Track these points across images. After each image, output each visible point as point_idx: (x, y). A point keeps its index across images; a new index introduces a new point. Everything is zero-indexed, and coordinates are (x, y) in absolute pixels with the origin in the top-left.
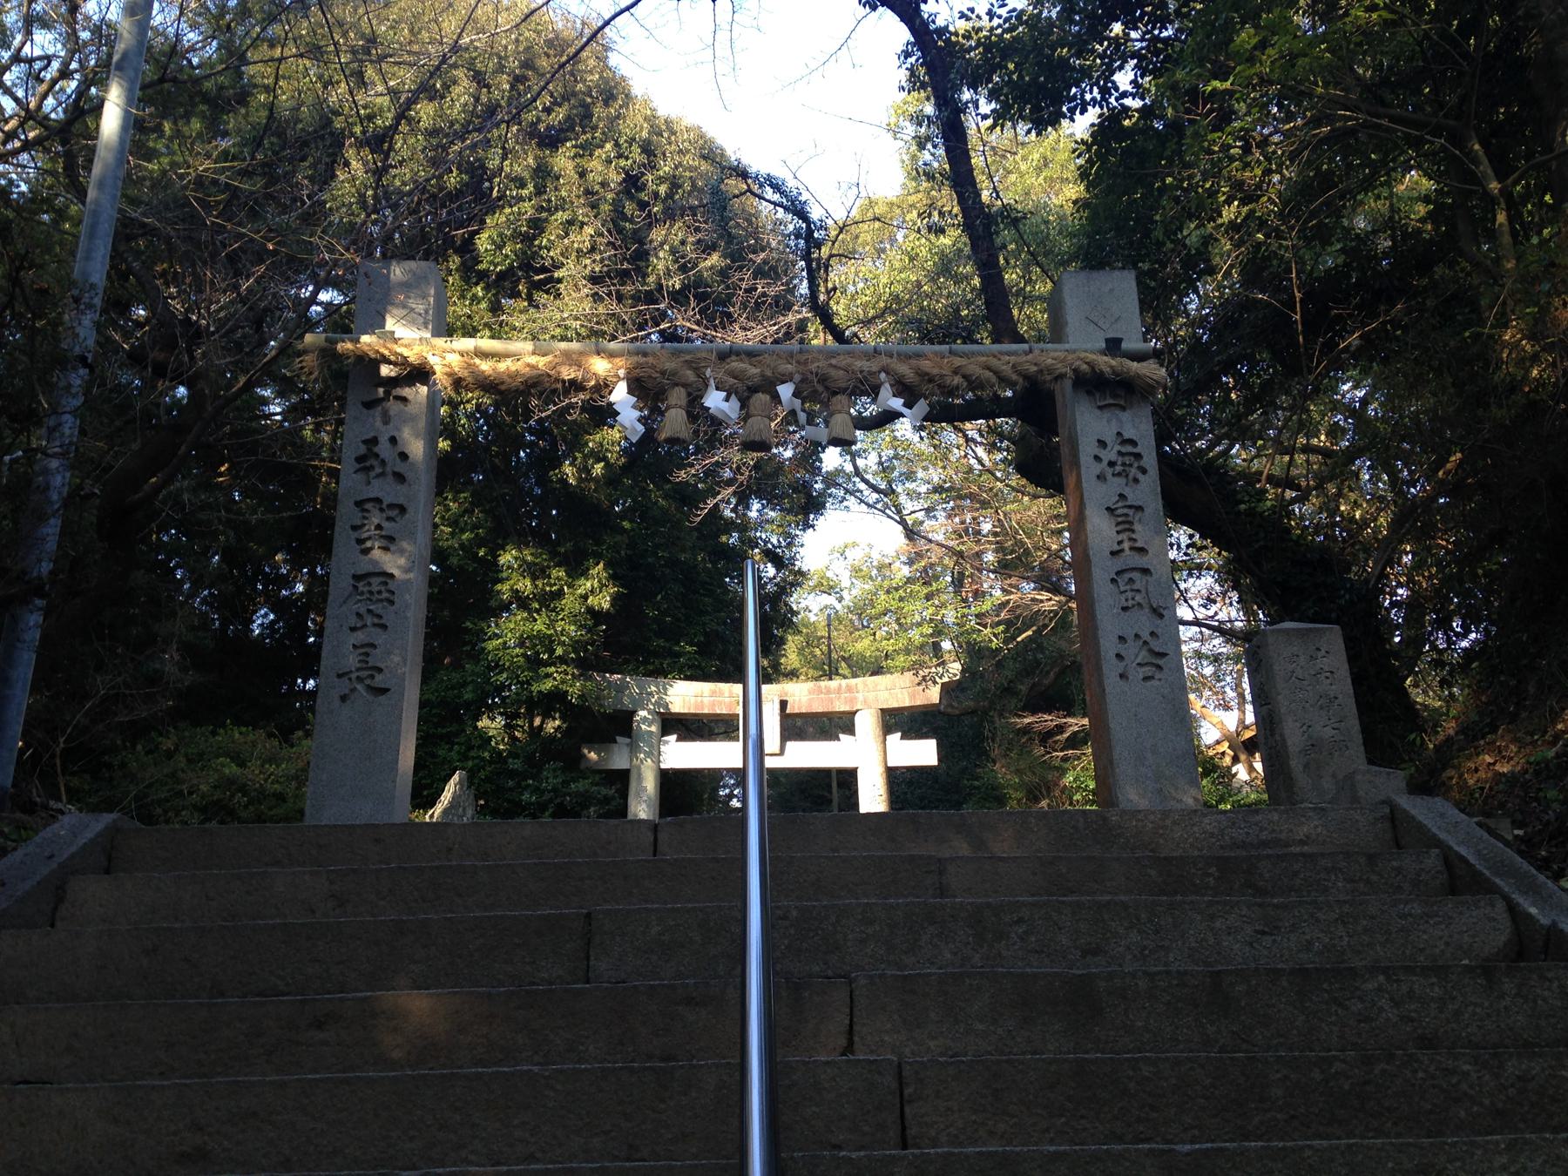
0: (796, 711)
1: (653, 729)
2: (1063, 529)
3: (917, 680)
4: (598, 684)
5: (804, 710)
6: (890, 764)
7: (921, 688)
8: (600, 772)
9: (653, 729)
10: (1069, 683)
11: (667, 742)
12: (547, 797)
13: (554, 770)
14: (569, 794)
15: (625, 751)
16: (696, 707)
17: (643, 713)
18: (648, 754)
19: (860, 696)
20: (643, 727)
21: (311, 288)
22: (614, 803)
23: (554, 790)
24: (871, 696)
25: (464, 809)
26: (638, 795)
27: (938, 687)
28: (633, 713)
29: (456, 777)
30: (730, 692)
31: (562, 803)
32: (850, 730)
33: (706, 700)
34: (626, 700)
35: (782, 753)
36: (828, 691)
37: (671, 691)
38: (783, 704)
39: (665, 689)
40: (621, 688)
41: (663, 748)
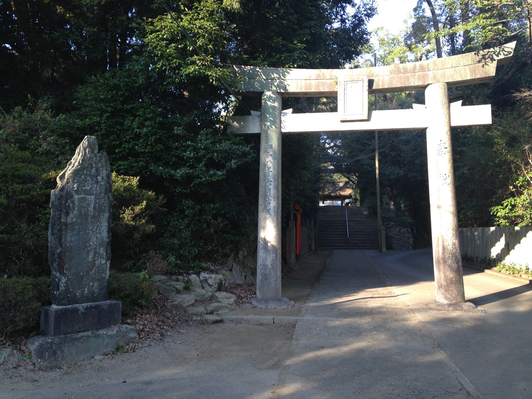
0: (381, 87)
1: (276, 104)
2: (171, 227)
3: (477, 58)
4: (235, 72)
5: (386, 86)
6: (452, 125)
7: (481, 64)
8: (241, 135)
9: (276, 104)
10: (520, 78)
11: (286, 114)
12: (202, 152)
13: (206, 135)
14: (217, 152)
15: (257, 121)
16: (306, 87)
17: (268, 93)
18: (273, 123)
19: (431, 74)
20: (269, 103)
21: (332, 167)
22: (250, 157)
23: (206, 148)
24: (439, 73)
25: (97, 170)
26: (266, 151)
27: (495, 64)
28: (261, 93)
29: (85, 142)
30: (331, 75)
31: (212, 157)
32: (421, 100)
33: (313, 83)
34: (257, 84)
35: (368, 120)
36: (406, 71)
37: (288, 77)
38: (371, 82)
39: (284, 76)
40: (253, 76)
41: (283, 118)
